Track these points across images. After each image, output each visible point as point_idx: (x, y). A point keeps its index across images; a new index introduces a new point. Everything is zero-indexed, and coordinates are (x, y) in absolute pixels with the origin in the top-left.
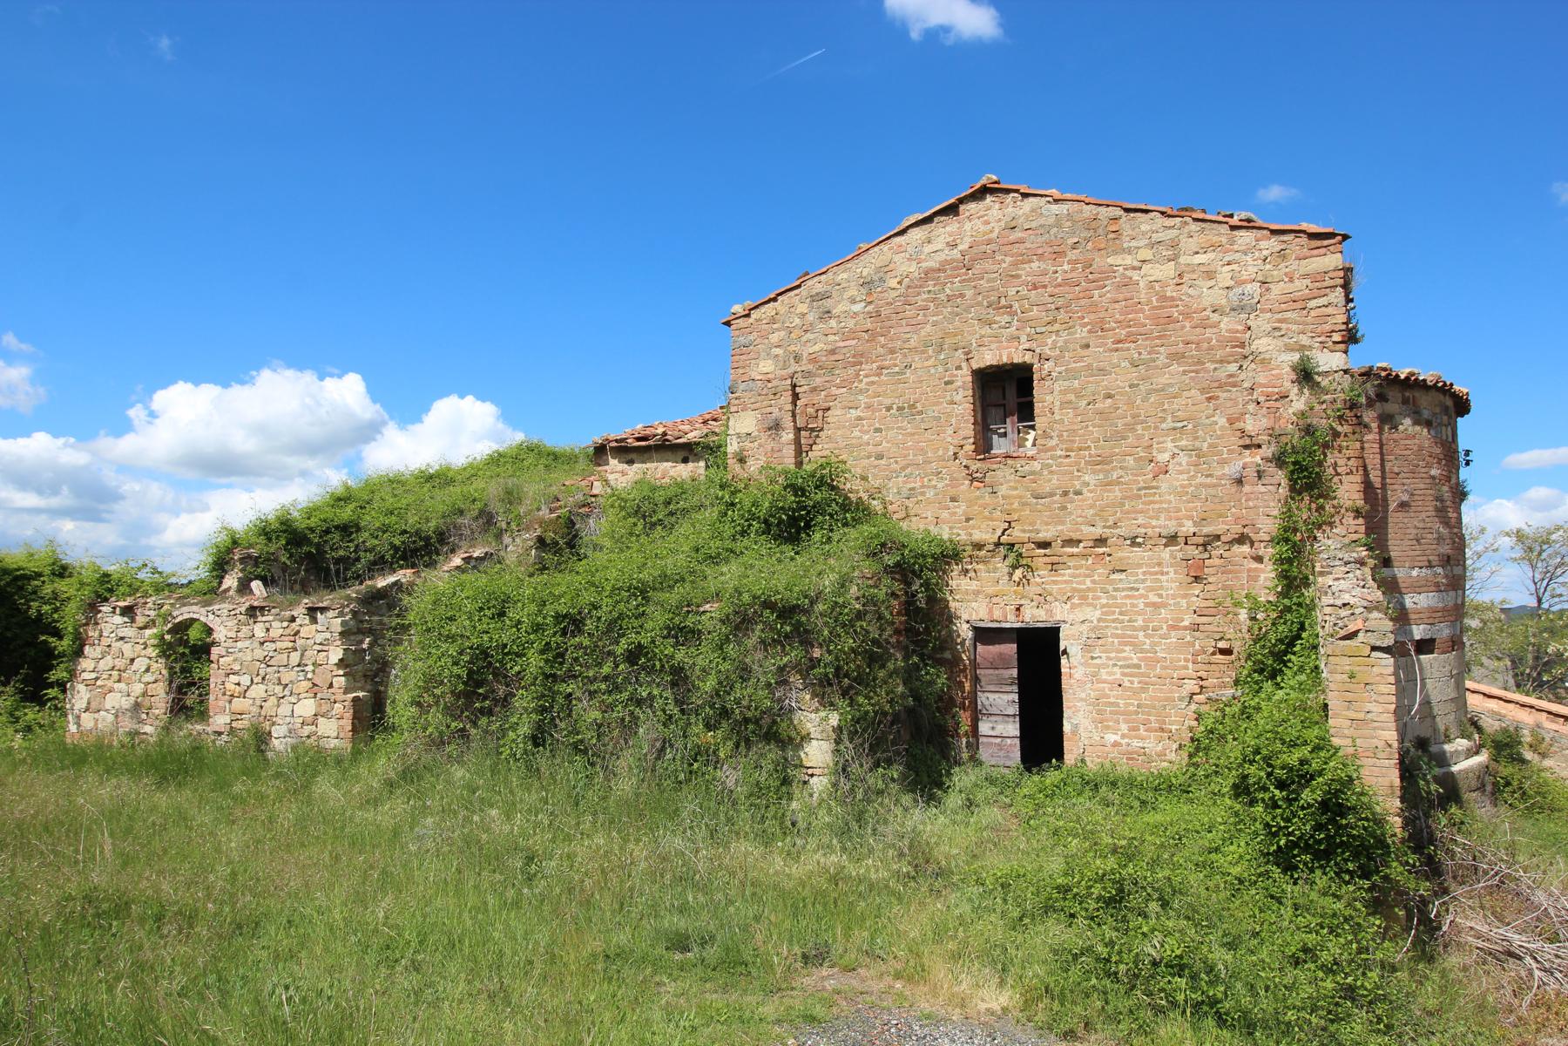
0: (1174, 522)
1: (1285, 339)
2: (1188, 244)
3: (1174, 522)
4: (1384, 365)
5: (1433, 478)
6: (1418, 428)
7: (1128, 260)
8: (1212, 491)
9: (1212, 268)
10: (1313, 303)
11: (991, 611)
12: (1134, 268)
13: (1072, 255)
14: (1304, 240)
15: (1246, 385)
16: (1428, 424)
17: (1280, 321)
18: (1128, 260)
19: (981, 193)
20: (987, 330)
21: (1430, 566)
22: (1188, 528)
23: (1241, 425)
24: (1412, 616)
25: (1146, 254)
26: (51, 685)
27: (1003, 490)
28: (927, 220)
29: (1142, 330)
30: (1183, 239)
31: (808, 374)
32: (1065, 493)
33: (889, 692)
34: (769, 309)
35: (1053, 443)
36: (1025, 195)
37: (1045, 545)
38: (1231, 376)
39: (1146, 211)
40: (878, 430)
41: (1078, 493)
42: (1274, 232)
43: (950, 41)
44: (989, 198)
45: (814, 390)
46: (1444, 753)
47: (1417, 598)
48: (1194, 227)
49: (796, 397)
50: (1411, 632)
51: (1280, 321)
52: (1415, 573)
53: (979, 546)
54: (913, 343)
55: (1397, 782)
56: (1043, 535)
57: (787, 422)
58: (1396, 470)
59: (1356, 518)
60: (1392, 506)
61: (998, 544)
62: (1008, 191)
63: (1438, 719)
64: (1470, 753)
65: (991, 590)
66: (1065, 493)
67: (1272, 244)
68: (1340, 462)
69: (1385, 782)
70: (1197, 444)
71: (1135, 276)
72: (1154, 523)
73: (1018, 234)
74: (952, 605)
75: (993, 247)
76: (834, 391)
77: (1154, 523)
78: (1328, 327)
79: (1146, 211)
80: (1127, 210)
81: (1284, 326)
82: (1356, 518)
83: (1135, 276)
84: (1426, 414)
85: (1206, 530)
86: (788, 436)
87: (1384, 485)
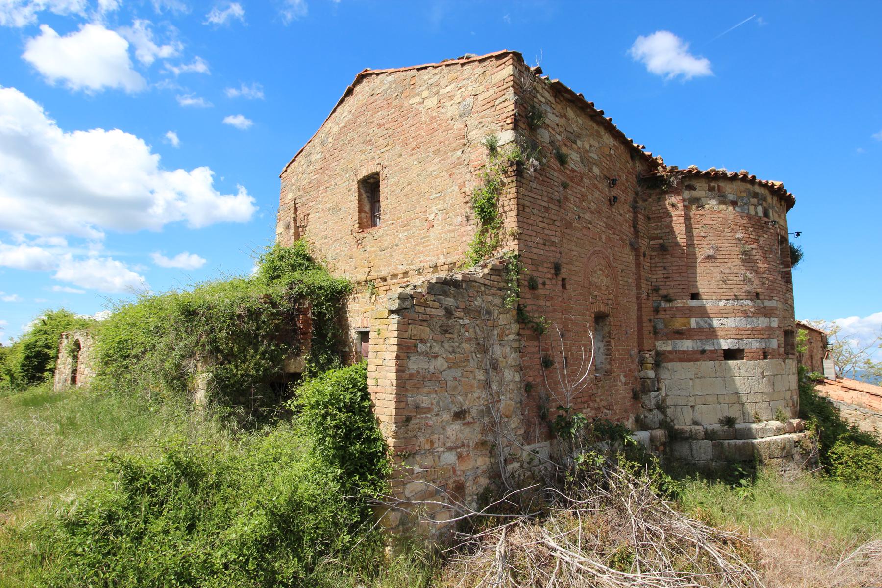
0: (435, 257)
1: (484, 128)
2: (444, 82)
3: (435, 257)
4: (713, 168)
5: (739, 239)
6: (723, 207)
7: (418, 99)
8: (452, 235)
9: (452, 93)
10: (498, 102)
11: (362, 323)
12: (420, 103)
13: (395, 103)
14: (494, 62)
15: (466, 162)
16: (734, 204)
17: (482, 117)
18: (418, 99)
19: (361, 78)
20: (363, 157)
21: (736, 298)
22: (441, 261)
23: (464, 189)
24: (720, 333)
25: (426, 94)
26: (47, 371)
27: (368, 249)
28: (342, 101)
29: (422, 140)
30: (442, 79)
31: (301, 197)
32: (392, 247)
33: (251, 365)
34: (292, 166)
35: (387, 217)
36: (378, 74)
37: (384, 279)
38: (458, 158)
39: (426, 68)
40: (325, 223)
41: (397, 246)
42: (481, 61)
43: (689, 77)
44: (365, 81)
45: (303, 205)
46: (750, 429)
47: (724, 321)
48: (446, 70)
49: (296, 210)
50: (719, 344)
51: (482, 117)
52: (722, 303)
53: (359, 283)
54: (338, 171)
55: (394, 412)
56: (384, 274)
57: (292, 225)
58: (703, 234)
59: (514, 239)
60: (700, 258)
61: (366, 281)
62: (371, 74)
63: (747, 405)
64: (778, 431)
65: (363, 309)
66: (392, 247)
67: (478, 69)
68: (506, 203)
69: (388, 411)
70: (446, 206)
71: (420, 108)
72: (427, 259)
73: (375, 97)
74: (349, 319)
75: (364, 108)
76: (311, 204)
77: (427, 259)
78: (505, 115)
79: (426, 68)
80: (418, 69)
81: (483, 120)
82: (514, 239)
83: (420, 108)
84: (731, 197)
85: (449, 260)
86: (292, 231)
87: (690, 244)
